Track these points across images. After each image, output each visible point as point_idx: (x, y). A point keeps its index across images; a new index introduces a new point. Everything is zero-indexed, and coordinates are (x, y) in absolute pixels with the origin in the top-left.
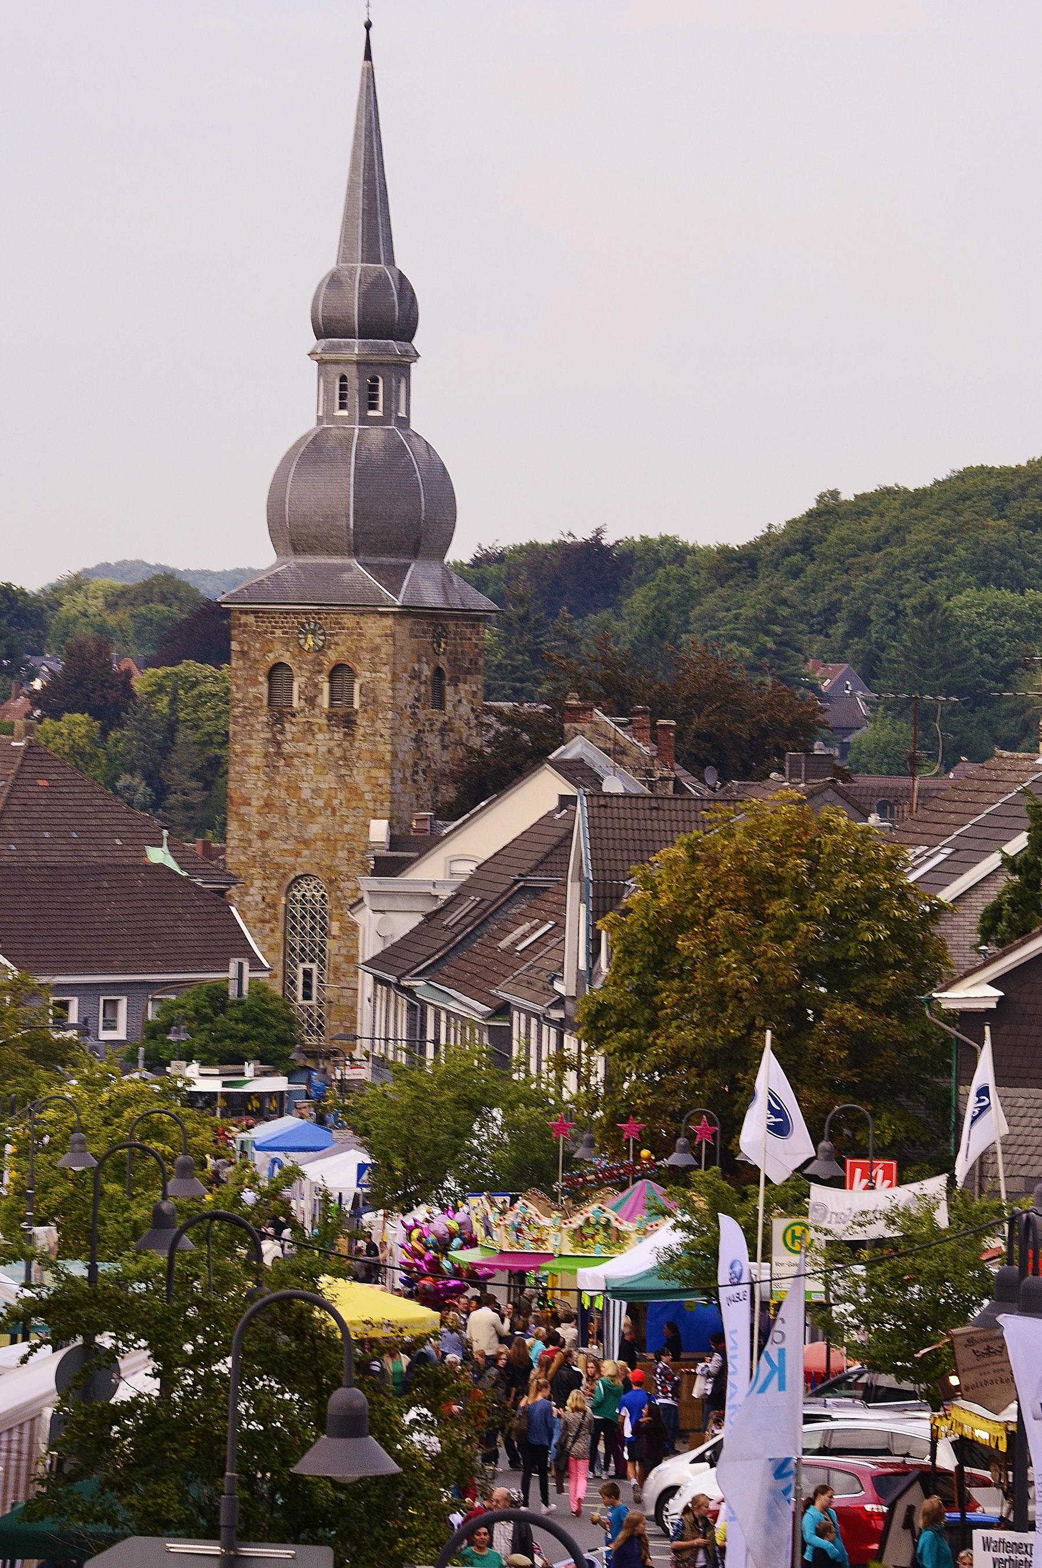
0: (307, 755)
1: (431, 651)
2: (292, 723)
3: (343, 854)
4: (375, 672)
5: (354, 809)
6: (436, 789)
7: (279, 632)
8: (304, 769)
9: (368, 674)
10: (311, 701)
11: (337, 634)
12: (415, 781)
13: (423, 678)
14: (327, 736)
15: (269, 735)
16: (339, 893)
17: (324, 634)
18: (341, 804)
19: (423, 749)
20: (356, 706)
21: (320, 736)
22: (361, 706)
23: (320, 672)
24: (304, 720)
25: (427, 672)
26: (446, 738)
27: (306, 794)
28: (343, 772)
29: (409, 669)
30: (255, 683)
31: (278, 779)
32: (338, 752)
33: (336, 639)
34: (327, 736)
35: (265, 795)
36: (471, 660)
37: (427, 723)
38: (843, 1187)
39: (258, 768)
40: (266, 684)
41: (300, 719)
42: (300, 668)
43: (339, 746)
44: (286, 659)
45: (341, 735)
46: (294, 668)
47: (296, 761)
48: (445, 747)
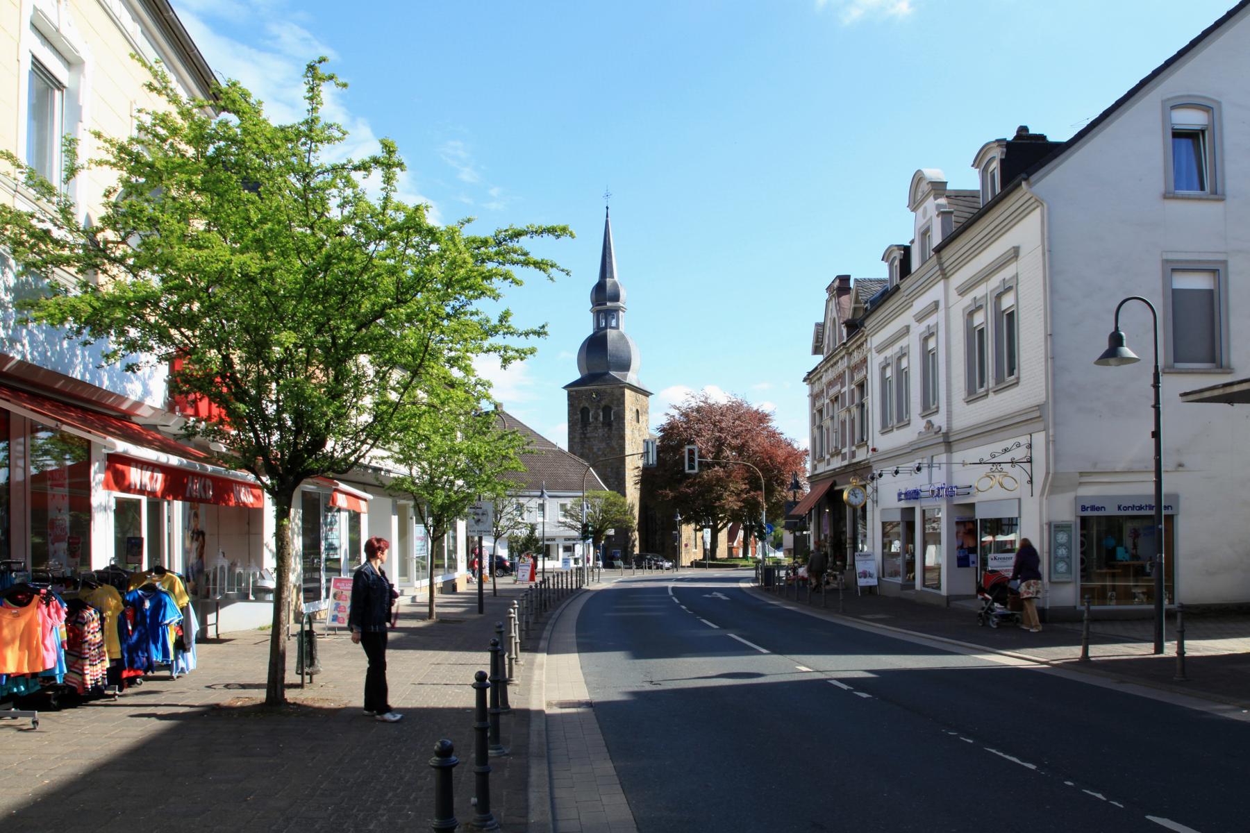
10: (596, 419)
20: (612, 418)
25: (634, 410)
27: (595, 450)
30: (577, 414)
32: (606, 435)
41: (592, 425)
44: (587, 405)
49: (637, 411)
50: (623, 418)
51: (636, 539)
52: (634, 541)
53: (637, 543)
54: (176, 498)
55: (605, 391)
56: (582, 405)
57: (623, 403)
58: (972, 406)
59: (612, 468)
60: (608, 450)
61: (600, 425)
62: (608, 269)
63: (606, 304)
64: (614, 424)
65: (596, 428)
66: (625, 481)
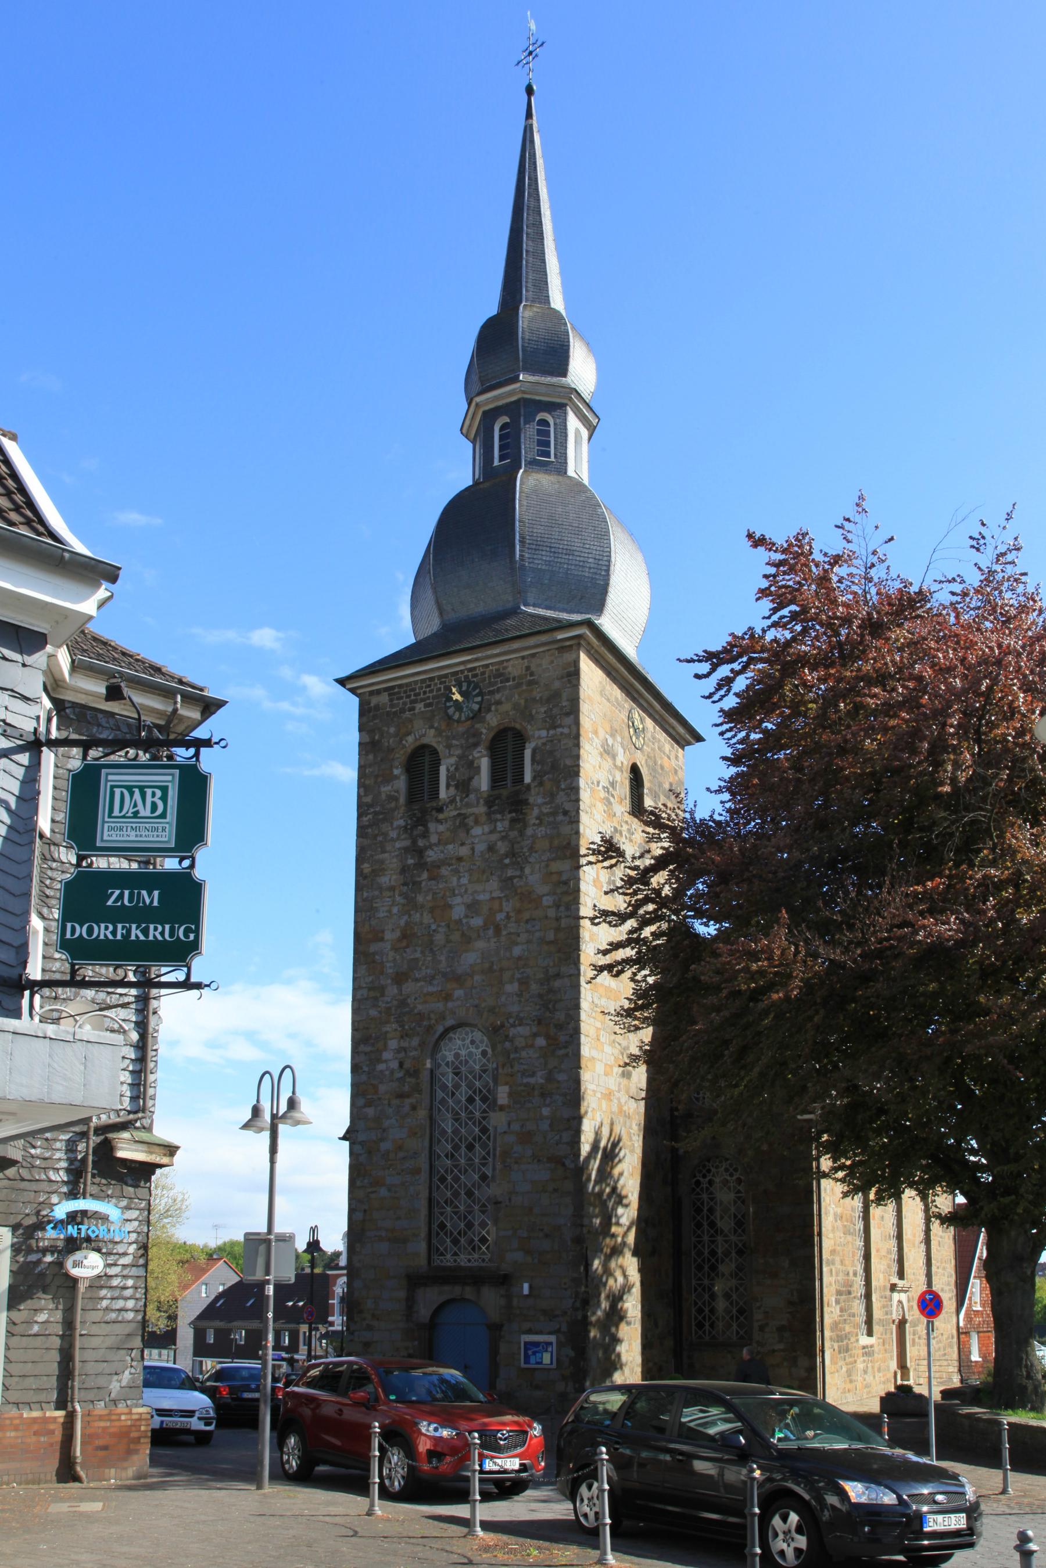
0: (460, 859)
3: (512, 988)
4: (555, 728)
5: (527, 922)
9: (544, 733)
10: (464, 786)
11: (498, 690)
14: (487, 829)
15: (407, 843)
16: (507, 1044)
17: (481, 694)
18: (508, 917)
20: (528, 778)
21: (477, 831)
22: (534, 779)
23: (476, 745)
24: (455, 813)
25: (624, 759)
27: (458, 912)
28: (510, 873)
30: (389, 778)
31: (420, 899)
32: (502, 847)
33: (497, 696)
34: (487, 829)
35: (402, 923)
39: (392, 889)
41: (450, 812)
43: (503, 838)
44: (430, 738)
45: (506, 823)
46: (440, 748)
47: (444, 871)
49: (635, 770)
50: (574, 771)
51: (626, 1288)
52: (616, 1299)
53: (633, 1306)
54: (656, 1022)
55: (500, 675)
56: (410, 741)
57: (574, 710)
58: (175, 1142)
59: (524, 982)
60: (507, 907)
61: (482, 809)
62: (527, 276)
63: (516, 380)
64: (536, 798)
65: (462, 823)
66: (577, 1032)
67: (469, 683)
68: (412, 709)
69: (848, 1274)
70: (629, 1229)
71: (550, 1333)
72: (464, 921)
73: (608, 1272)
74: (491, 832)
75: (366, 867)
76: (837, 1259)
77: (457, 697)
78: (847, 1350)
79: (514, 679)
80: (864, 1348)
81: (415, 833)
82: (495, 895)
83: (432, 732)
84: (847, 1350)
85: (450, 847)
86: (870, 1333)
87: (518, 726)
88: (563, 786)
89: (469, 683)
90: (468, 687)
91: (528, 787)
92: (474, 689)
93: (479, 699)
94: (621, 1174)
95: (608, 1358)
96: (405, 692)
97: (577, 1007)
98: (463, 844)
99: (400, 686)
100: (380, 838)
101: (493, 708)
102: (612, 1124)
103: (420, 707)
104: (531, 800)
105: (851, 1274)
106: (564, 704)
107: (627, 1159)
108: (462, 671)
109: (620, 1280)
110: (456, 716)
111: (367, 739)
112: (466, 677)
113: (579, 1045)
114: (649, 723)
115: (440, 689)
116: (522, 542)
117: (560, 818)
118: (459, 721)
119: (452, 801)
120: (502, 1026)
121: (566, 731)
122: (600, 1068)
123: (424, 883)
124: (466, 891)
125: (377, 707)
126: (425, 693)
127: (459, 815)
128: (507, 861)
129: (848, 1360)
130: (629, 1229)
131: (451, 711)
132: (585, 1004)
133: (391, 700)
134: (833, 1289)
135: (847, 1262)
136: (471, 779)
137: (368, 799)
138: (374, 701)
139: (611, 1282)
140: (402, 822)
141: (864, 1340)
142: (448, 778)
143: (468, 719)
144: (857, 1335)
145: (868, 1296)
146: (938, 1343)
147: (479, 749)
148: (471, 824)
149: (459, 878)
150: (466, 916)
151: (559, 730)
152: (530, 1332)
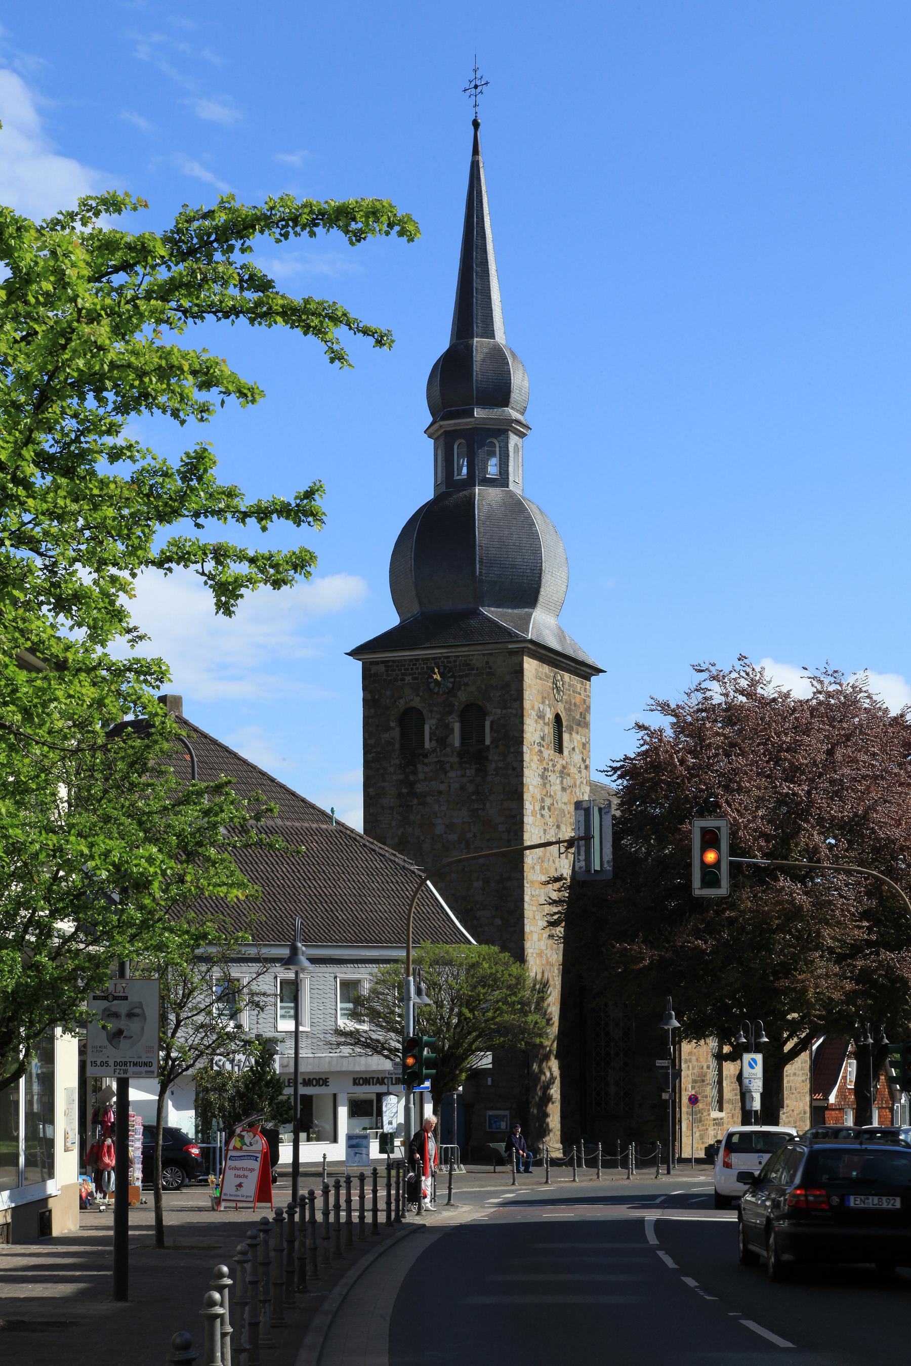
0: (440, 793)
1: (552, 695)
2: (424, 764)
3: (478, 884)
4: (506, 708)
5: (488, 840)
6: (558, 827)
7: (408, 679)
8: (436, 807)
9: (499, 711)
10: (442, 741)
11: (466, 675)
12: (542, 816)
13: (547, 720)
14: (459, 773)
15: (402, 777)
16: (475, 922)
17: (453, 676)
18: (475, 836)
19: (548, 786)
20: (488, 742)
21: (452, 774)
22: (492, 742)
23: (450, 713)
24: (436, 760)
25: (549, 716)
26: (565, 781)
27: (439, 830)
28: (476, 806)
29: (536, 708)
30: (388, 729)
31: (412, 817)
32: (470, 788)
33: (466, 680)
34: (459, 773)
35: (399, 833)
36: (581, 714)
37: (551, 763)
38: (81, 1208)
39: (391, 808)
40: (398, 729)
41: (432, 759)
42: (431, 711)
43: (471, 781)
44: (417, 702)
45: (473, 771)
46: (425, 712)
47: (429, 800)
48: (564, 789)
51: (552, 1080)
52: (547, 1086)
53: (555, 1091)
61: (455, 759)
62: (478, 312)
66: (521, 917)
67: (445, 667)
68: (403, 680)
69: (702, 1068)
70: (553, 1042)
71: (507, 1109)
72: (444, 836)
73: (542, 1072)
74: (463, 776)
75: (371, 791)
76: (694, 1058)
77: (437, 677)
78: (700, 1121)
79: (477, 669)
80: (714, 1120)
81: (407, 770)
82: (466, 820)
83: (418, 699)
84: (700, 1121)
85: (434, 783)
86: (721, 1110)
87: (480, 704)
88: (512, 750)
89: (445, 667)
90: (445, 670)
91: (488, 746)
92: (449, 672)
93: (452, 680)
94: (549, 1005)
95: (541, 1126)
96: (397, 666)
97: (522, 900)
98: (442, 782)
99: (393, 661)
100: (382, 771)
101: (463, 688)
102: (543, 973)
103: (408, 679)
104: (490, 757)
105: (705, 1067)
106: (513, 692)
107: (553, 994)
108: (440, 658)
109: (548, 1074)
110: (436, 690)
111: (369, 697)
112: (443, 662)
113: (523, 925)
114: (567, 676)
115: (423, 668)
116: (481, 562)
117: (510, 772)
118: (438, 694)
119: (434, 751)
120: (472, 909)
121: (514, 711)
122: (535, 937)
123: (414, 807)
124: (445, 815)
125: (376, 674)
126: (412, 669)
127: (439, 761)
128: (474, 797)
129: (701, 1128)
130: (553, 1042)
131: (432, 685)
132: (527, 898)
133: (387, 671)
134: (690, 1079)
135: (701, 1060)
136: (447, 737)
137: (372, 742)
138: (374, 669)
139: (543, 1078)
140: (397, 762)
141: (715, 1114)
142: (430, 734)
143: (444, 693)
144: (709, 1110)
145: (720, 1082)
146: (787, 1117)
147: (453, 716)
148: (448, 769)
149: (440, 806)
150: (446, 833)
151: (510, 710)
152: (492, 1109)
